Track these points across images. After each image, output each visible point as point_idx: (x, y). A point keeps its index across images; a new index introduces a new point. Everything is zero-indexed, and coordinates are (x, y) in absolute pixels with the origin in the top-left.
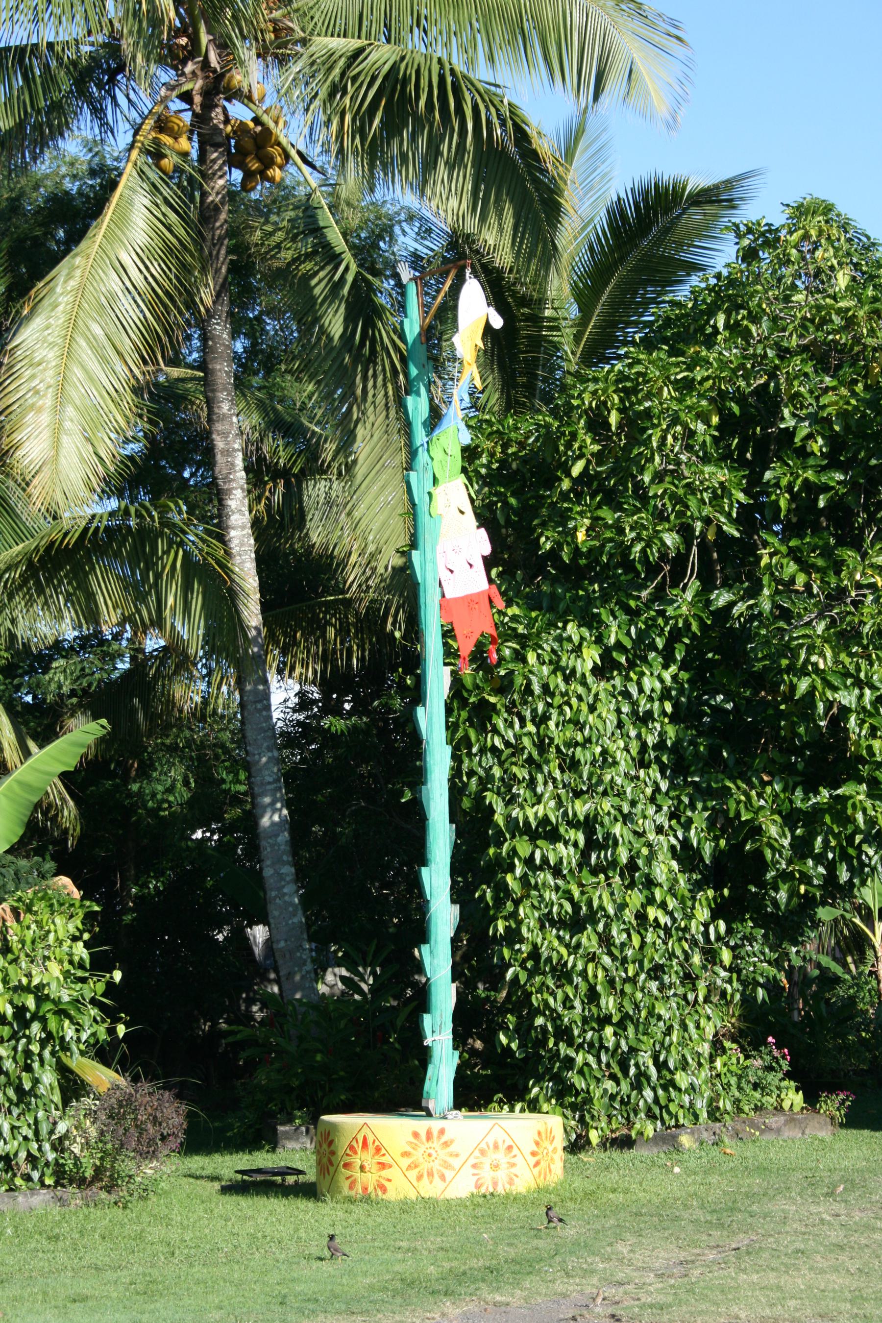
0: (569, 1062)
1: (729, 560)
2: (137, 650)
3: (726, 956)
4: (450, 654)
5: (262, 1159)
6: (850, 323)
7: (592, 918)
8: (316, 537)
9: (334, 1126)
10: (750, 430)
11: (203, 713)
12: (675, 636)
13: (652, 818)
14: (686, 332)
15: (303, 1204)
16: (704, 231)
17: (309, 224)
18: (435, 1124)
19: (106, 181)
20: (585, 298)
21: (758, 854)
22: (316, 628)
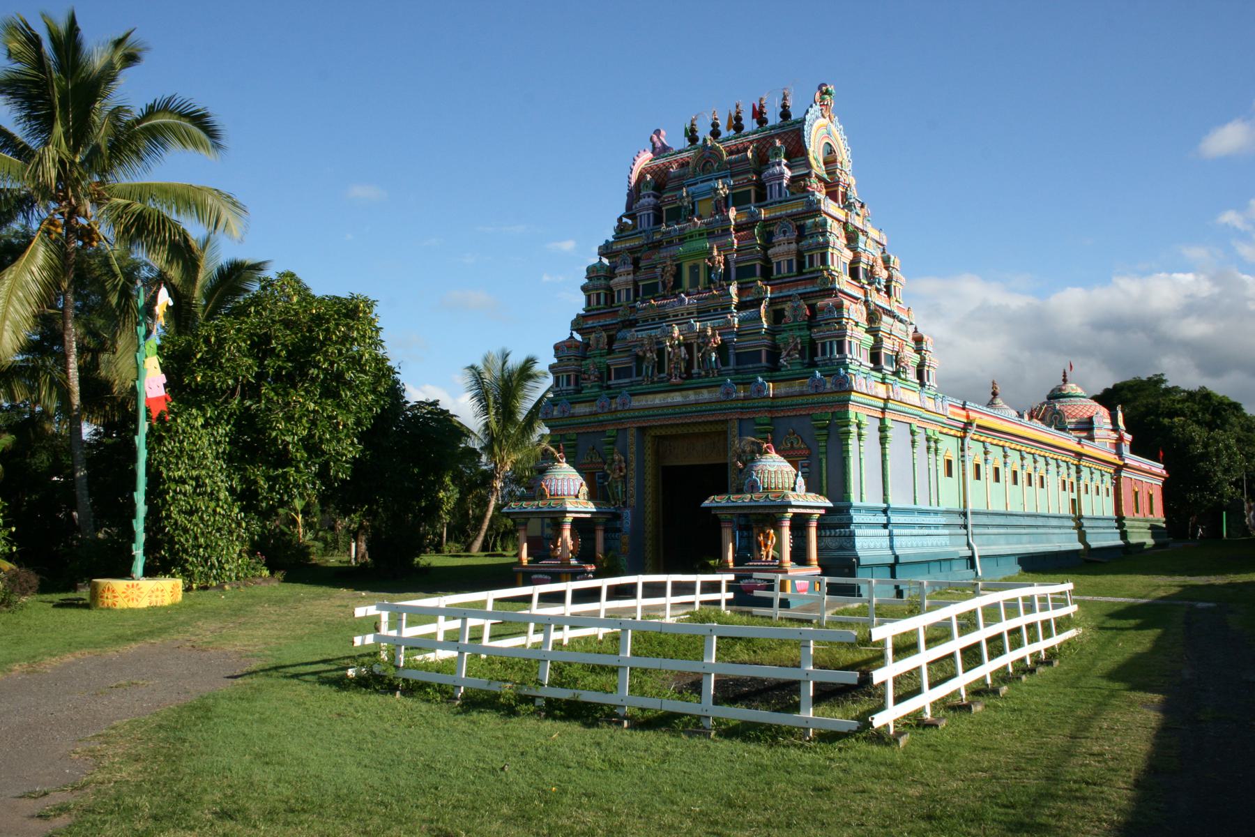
0: (187, 561)
1: (251, 391)
2: (32, 411)
3: (244, 525)
4: (148, 417)
5: (71, 595)
6: (297, 314)
7: (197, 511)
8: (103, 374)
9: (97, 584)
10: (260, 346)
11: (55, 435)
12: (231, 415)
13: (220, 477)
14: (241, 312)
15: (85, 611)
16: (250, 279)
17: (106, 262)
18: (135, 582)
19: (28, 239)
20: (208, 296)
21: (256, 490)
22: (103, 406)
